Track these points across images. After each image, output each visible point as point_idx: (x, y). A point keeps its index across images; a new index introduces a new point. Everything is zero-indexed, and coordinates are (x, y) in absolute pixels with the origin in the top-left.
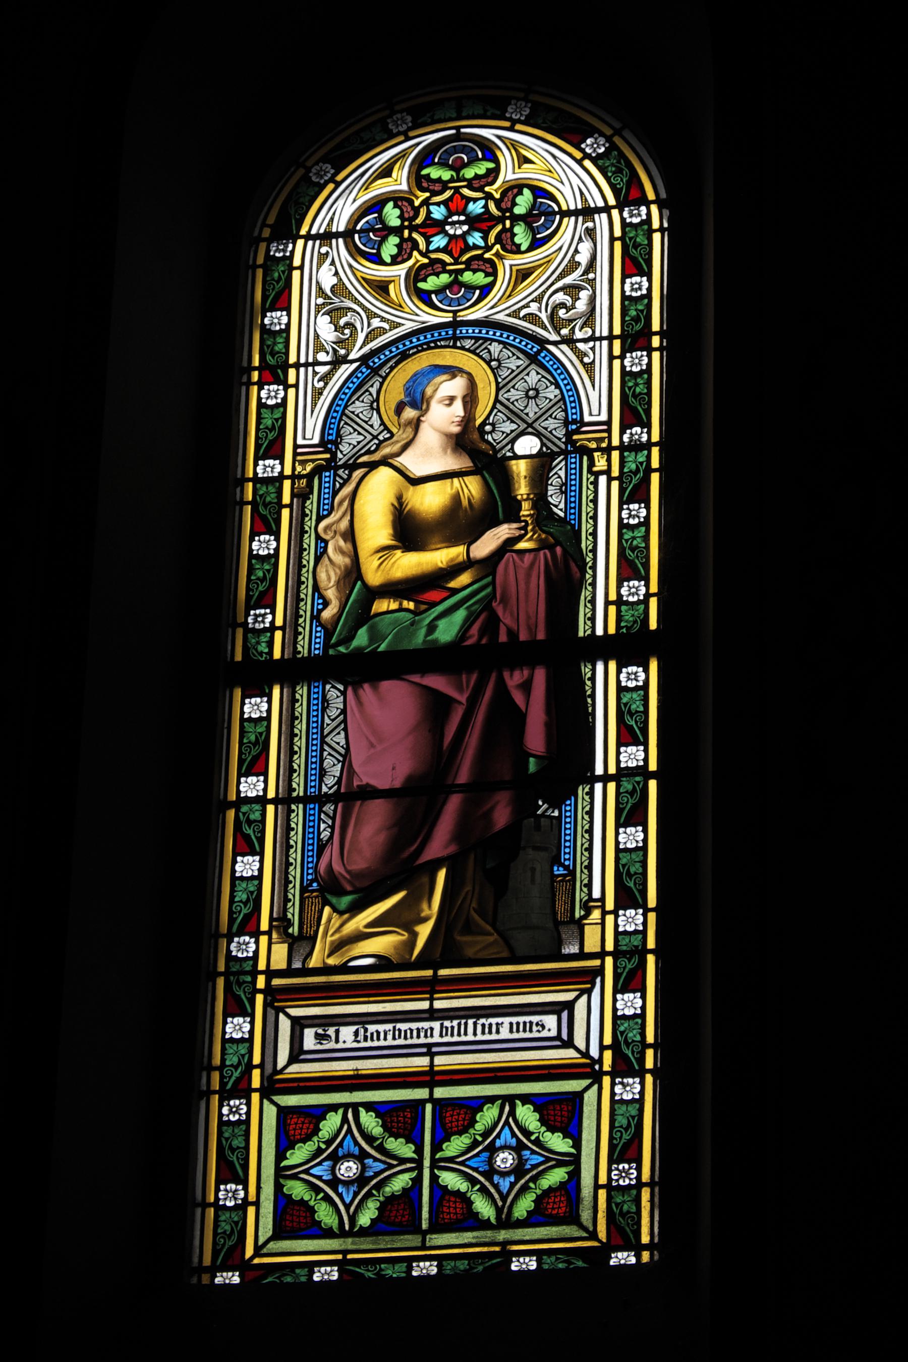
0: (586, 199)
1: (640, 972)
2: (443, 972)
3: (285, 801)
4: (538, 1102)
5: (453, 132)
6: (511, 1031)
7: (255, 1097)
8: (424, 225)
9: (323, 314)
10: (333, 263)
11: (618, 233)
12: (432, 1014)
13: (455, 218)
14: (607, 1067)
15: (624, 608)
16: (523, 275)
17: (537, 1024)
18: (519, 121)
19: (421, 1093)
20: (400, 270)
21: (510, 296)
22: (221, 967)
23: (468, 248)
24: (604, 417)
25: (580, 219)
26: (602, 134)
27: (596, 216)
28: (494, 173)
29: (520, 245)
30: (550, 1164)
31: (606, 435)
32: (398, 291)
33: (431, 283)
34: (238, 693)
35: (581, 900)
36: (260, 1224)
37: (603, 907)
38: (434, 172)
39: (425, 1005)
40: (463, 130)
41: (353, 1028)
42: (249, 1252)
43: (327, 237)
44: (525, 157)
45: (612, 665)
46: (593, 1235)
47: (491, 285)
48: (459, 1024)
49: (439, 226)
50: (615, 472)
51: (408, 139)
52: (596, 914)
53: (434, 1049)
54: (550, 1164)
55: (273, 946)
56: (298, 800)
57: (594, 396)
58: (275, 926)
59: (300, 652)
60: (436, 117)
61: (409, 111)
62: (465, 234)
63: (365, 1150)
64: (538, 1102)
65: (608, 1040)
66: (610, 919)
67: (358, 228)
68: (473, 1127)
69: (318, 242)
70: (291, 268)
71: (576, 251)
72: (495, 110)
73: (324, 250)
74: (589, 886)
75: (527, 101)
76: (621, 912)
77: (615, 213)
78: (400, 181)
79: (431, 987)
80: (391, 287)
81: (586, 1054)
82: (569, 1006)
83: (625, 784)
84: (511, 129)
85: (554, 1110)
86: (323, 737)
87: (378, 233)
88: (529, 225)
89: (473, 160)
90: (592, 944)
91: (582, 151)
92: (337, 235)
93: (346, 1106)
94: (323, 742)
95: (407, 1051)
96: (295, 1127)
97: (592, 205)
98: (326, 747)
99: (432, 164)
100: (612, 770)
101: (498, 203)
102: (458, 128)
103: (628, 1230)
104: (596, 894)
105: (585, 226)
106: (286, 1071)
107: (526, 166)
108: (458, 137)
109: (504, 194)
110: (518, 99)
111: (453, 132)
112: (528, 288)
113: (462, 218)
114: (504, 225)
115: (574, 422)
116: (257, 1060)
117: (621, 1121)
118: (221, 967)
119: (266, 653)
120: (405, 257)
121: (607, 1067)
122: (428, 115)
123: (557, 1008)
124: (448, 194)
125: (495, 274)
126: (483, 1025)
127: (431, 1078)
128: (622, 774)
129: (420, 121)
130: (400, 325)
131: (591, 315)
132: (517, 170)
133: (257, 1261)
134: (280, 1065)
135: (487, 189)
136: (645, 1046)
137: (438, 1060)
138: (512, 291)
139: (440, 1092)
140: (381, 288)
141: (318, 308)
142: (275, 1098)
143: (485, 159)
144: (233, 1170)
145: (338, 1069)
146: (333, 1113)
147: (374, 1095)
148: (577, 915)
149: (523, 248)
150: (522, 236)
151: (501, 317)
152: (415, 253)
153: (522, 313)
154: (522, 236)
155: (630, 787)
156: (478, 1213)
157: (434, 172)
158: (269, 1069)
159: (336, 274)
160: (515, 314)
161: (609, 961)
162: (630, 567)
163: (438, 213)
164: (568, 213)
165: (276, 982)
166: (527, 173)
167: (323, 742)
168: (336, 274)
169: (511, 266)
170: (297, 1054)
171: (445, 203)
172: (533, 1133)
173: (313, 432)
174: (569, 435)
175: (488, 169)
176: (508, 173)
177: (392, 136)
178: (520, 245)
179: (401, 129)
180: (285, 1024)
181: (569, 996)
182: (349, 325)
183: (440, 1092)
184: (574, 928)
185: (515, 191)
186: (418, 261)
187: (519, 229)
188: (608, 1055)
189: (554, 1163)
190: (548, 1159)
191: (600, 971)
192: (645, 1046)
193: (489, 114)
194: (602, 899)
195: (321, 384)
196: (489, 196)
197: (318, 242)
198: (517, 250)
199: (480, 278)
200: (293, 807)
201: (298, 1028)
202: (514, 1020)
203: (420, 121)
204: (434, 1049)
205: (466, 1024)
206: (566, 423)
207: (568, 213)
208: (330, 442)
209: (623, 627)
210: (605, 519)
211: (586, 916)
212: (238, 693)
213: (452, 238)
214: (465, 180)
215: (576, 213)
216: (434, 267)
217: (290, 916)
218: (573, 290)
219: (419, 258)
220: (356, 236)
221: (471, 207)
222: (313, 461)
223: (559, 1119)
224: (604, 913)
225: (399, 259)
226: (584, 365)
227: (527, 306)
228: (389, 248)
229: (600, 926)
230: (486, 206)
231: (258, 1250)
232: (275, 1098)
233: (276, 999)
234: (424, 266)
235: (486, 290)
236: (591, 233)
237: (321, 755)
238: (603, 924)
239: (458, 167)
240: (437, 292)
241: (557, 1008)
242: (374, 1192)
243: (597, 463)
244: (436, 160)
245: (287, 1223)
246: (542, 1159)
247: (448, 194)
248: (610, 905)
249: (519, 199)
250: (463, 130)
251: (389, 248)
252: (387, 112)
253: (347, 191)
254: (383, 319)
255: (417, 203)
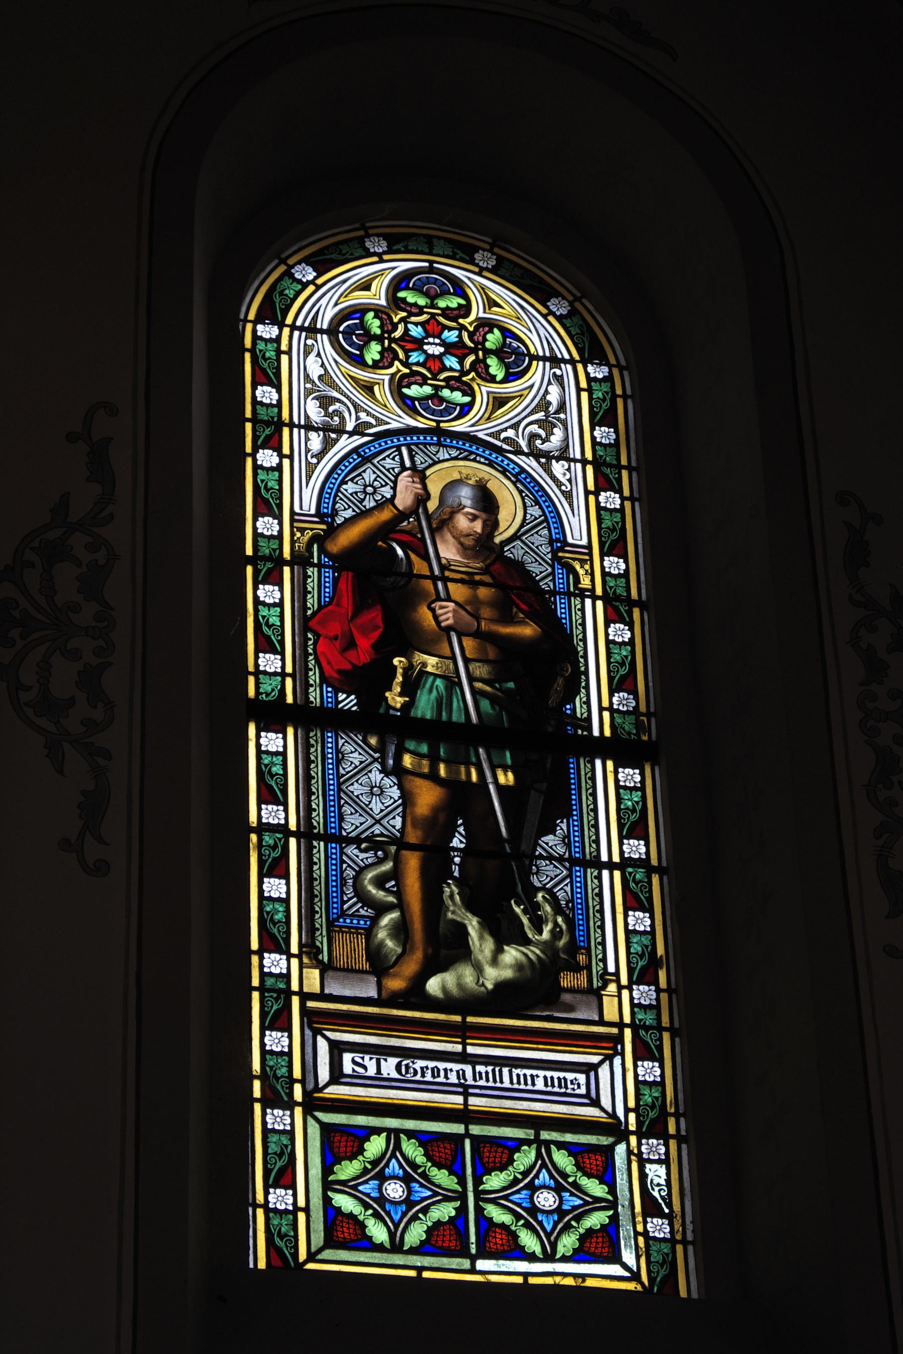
0: (553, 349)
1: (285, 1013)
2: (470, 1019)
3: (306, 834)
4: (424, 1139)
5: (427, 264)
6: (546, 1085)
7: (298, 1111)
8: (402, 338)
9: (313, 399)
10: (319, 355)
11: (583, 384)
12: (463, 1058)
13: (431, 340)
14: (632, 1127)
15: (261, 676)
16: (499, 402)
17: (572, 1082)
18: (487, 269)
19: (457, 1128)
20: (384, 375)
21: (489, 418)
22: (255, 982)
23: (444, 369)
24: (584, 542)
25: (548, 364)
26: (564, 298)
27: (319, 336)
28: (465, 310)
29: (495, 376)
30: (438, 1198)
31: (587, 557)
32: (383, 393)
33: (414, 391)
34: (252, 729)
35: (597, 972)
36: (308, 1234)
37: (618, 981)
38: (410, 297)
39: (459, 1048)
40: (435, 265)
41: (397, 1060)
42: (303, 1255)
43: (312, 330)
44: (494, 301)
45: (610, 765)
46: (311, 1257)
47: (471, 405)
48: (494, 1071)
49: (419, 344)
50: (599, 591)
51: (381, 261)
52: (612, 988)
53: (471, 1091)
54: (438, 1198)
55: (305, 970)
56: (319, 837)
57: (574, 521)
58: (305, 952)
59: (312, 702)
60: (410, 248)
61: (386, 237)
62: (442, 355)
63: (376, 1174)
64: (424, 1139)
65: (632, 1104)
66: (625, 993)
67: (341, 329)
68: (584, 1175)
69: (304, 334)
70: (279, 352)
71: (547, 392)
72: (465, 254)
73: (309, 342)
74: (604, 960)
75: (493, 254)
76: (266, 955)
77: (580, 367)
78: (378, 295)
79: (463, 1032)
80: (376, 388)
81: (613, 1115)
82: (595, 1067)
83: (267, 838)
84: (479, 274)
85: (438, 1147)
86: (339, 784)
87: (361, 338)
88: (501, 359)
89: (444, 293)
90: (610, 1013)
91: (547, 307)
92: (322, 331)
93: (389, 1131)
94: (340, 790)
95: (445, 1088)
96: (339, 1144)
97: (559, 356)
98: (342, 795)
99: (407, 288)
100: (616, 858)
101: (471, 335)
102: (431, 262)
103: (286, 1252)
104: (611, 968)
105: (553, 371)
106: (325, 1091)
107: (495, 309)
108: (431, 270)
109: (477, 328)
110: (484, 250)
111: (427, 264)
112: (504, 416)
113: (437, 341)
114: (477, 355)
115: (558, 540)
116: (297, 1073)
117: (273, 1148)
118: (255, 982)
119: (634, 734)
120: (386, 364)
121: (632, 1127)
122: (402, 244)
123: (584, 1068)
124: (424, 317)
125: (473, 395)
126: (518, 1075)
127: (465, 1115)
128: (625, 863)
129: (394, 248)
130: (388, 423)
131: (565, 451)
132: (487, 311)
133: (311, 1266)
134: (321, 1083)
135: (461, 321)
136: (293, 1081)
137: (472, 1100)
138: (491, 414)
139: (475, 1130)
140: (368, 388)
141: (308, 393)
142: (317, 1114)
143: (456, 294)
144: (283, 1177)
145: (520, 1108)
146: (376, 1136)
147: (482, 1130)
148: (595, 986)
149: (499, 378)
150: (495, 367)
151: (481, 435)
152: (397, 363)
153: (503, 435)
154: (495, 367)
155: (271, 842)
156: (371, 1237)
157: (410, 297)
158: (310, 1086)
159: (323, 365)
160: (496, 435)
161: (628, 1032)
162: (621, 681)
163: (416, 332)
164: (537, 358)
165: (310, 1004)
166: (493, 314)
167: (340, 790)
168: (323, 365)
169: (488, 393)
170: (337, 1076)
171: (423, 324)
172: (420, 1167)
173: (309, 502)
174: (554, 552)
175: (459, 304)
176: (477, 311)
177: (369, 254)
178: (495, 376)
179: (481, 264)
180: (323, 1046)
181: (595, 1059)
182: (337, 413)
183: (475, 1130)
184: (593, 999)
185: (487, 329)
186: (399, 371)
187: (492, 361)
188: (632, 1117)
189: (440, 1197)
190: (436, 1194)
191: (620, 1039)
192: (293, 1081)
193: (458, 256)
194: (617, 973)
195: (314, 461)
196: (462, 328)
197: (304, 334)
198: (492, 379)
199: (458, 397)
200: (315, 843)
201: (336, 1051)
202: (549, 1074)
203: (394, 248)
204: (471, 1091)
205: (501, 1072)
206: (551, 542)
207: (537, 358)
208: (327, 515)
209: (262, 694)
210: (598, 636)
211: (604, 987)
212: (252, 729)
213: (429, 357)
214: (438, 308)
215: (544, 359)
216: (412, 378)
217: (318, 944)
218: (547, 425)
219: (401, 368)
220: (340, 335)
221: (446, 334)
222: (312, 529)
223: (491, 1160)
224: (620, 988)
225: (381, 365)
226: (563, 492)
227: (505, 430)
228: (373, 352)
229: (616, 999)
230: (460, 336)
231: (311, 1257)
232: (317, 1114)
233: (315, 1021)
234: (405, 376)
235: (466, 409)
236: (559, 380)
237: (339, 802)
238: (619, 996)
239: (433, 298)
240: (419, 399)
241: (584, 1068)
242: (420, 1215)
243: (582, 582)
244: (411, 285)
245: (492, 1244)
246: (360, 1188)
247: (424, 317)
248: (624, 981)
249: (377, 322)
250: (435, 265)
251: (373, 352)
252: (488, 247)
253: (534, 320)
254: (369, 414)
255: (396, 320)
